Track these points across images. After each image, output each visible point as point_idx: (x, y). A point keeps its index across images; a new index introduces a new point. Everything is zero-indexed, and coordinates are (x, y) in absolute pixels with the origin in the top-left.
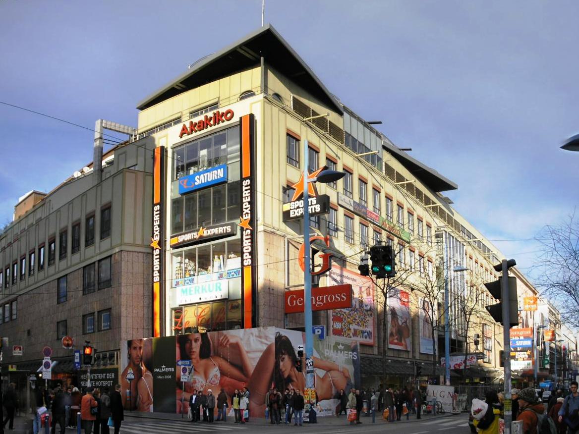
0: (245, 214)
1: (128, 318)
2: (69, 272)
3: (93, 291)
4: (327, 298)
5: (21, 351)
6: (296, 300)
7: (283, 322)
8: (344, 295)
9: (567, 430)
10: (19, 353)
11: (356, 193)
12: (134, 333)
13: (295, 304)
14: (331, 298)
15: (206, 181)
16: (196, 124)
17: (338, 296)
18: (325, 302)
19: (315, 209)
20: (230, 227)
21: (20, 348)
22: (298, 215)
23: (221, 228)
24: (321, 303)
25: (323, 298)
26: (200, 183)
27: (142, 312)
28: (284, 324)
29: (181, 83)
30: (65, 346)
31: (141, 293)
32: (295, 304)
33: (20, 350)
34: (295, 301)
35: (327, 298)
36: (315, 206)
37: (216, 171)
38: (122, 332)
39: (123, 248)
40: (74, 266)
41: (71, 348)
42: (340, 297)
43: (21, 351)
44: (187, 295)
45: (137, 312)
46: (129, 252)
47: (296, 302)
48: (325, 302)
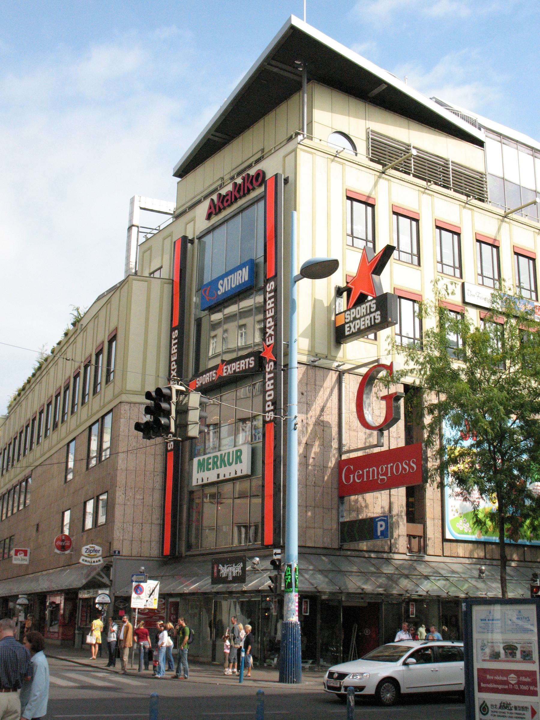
0: (268, 337)
1: (126, 507)
2: (78, 433)
3: (459, 317)
4: (392, 468)
5: (27, 558)
6: (353, 472)
7: (334, 512)
8: (413, 462)
9: (242, 651)
10: (22, 560)
11: (72, 454)
12: (136, 531)
13: (352, 481)
14: (397, 467)
15: (229, 288)
16: (224, 196)
17: (406, 464)
18: (389, 475)
19: (375, 319)
20: (253, 358)
21: (25, 553)
22: (354, 331)
23: (243, 361)
24: (385, 477)
25: (387, 468)
26: (224, 291)
27: (151, 498)
28: (338, 516)
29: (216, 131)
30: (58, 549)
31: (150, 467)
32: (352, 481)
33: (26, 555)
34: (352, 476)
35: (392, 468)
36: (373, 314)
37: (240, 271)
38: (116, 527)
39: (124, 398)
40: (95, 414)
41: (67, 552)
42: (409, 465)
43: (27, 558)
44: (204, 471)
45: (142, 498)
46: (132, 405)
47: (354, 477)
48: (389, 475)
